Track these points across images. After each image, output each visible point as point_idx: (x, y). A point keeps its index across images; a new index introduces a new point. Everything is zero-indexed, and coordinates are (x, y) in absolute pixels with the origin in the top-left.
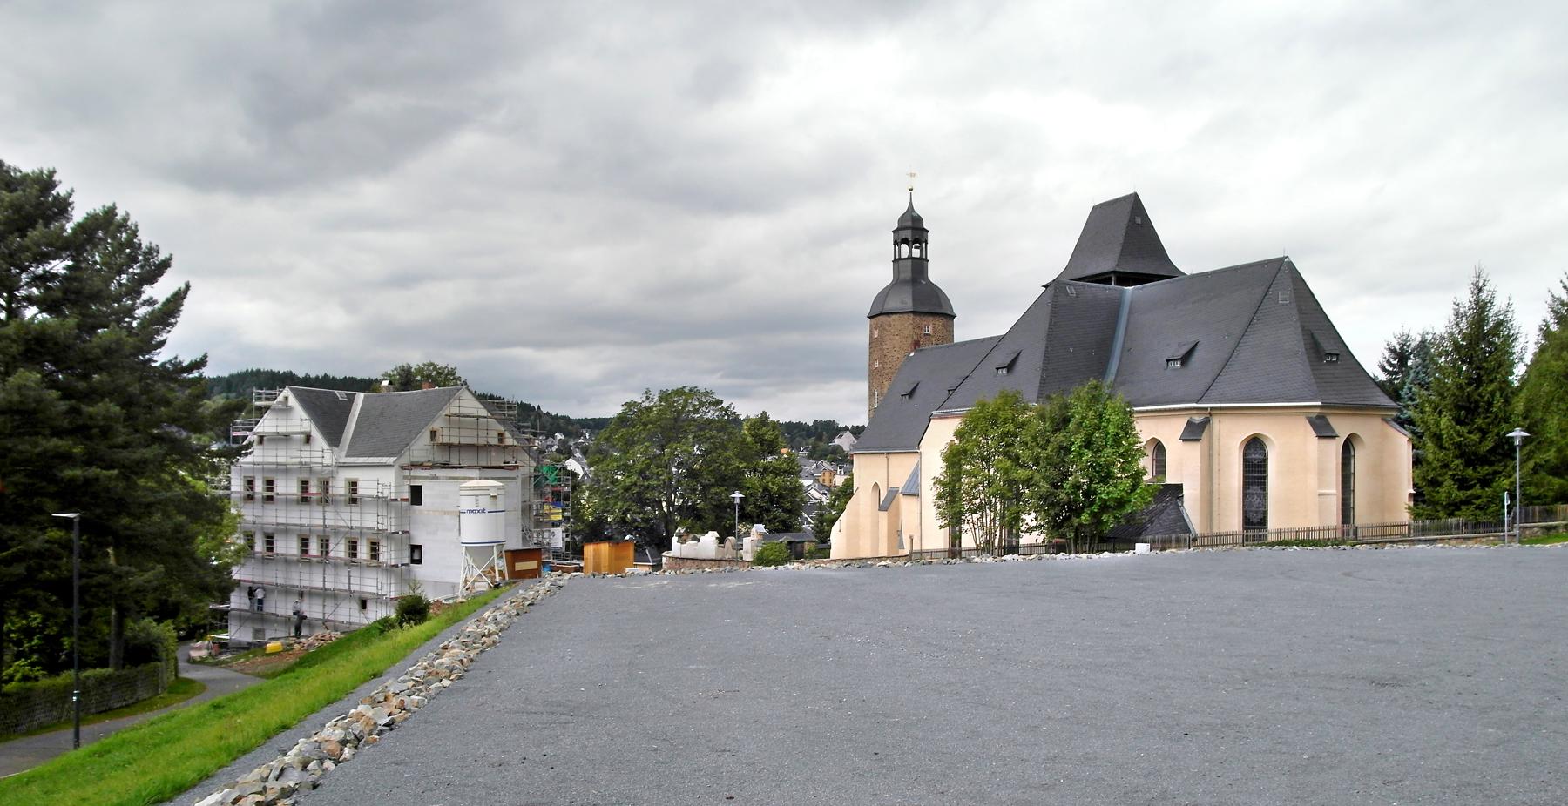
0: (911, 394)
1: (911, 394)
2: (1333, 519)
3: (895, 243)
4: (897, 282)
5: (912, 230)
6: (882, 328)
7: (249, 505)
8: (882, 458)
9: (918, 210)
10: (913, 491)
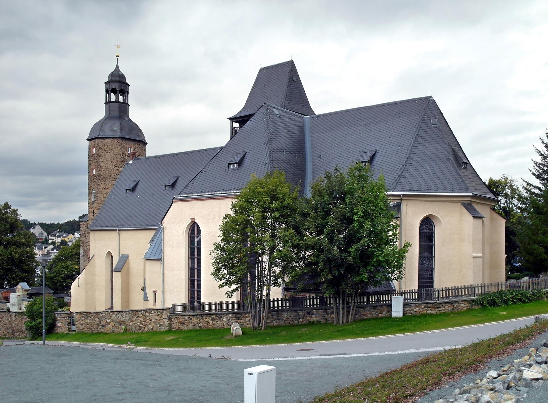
0: (134, 189)
1: (134, 189)
2: (481, 259)
3: (107, 92)
4: (108, 117)
5: (117, 85)
6: (98, 148)
7: (271, 237)
8: (114, 235)
9: (123, 70)
10: (156, 257)
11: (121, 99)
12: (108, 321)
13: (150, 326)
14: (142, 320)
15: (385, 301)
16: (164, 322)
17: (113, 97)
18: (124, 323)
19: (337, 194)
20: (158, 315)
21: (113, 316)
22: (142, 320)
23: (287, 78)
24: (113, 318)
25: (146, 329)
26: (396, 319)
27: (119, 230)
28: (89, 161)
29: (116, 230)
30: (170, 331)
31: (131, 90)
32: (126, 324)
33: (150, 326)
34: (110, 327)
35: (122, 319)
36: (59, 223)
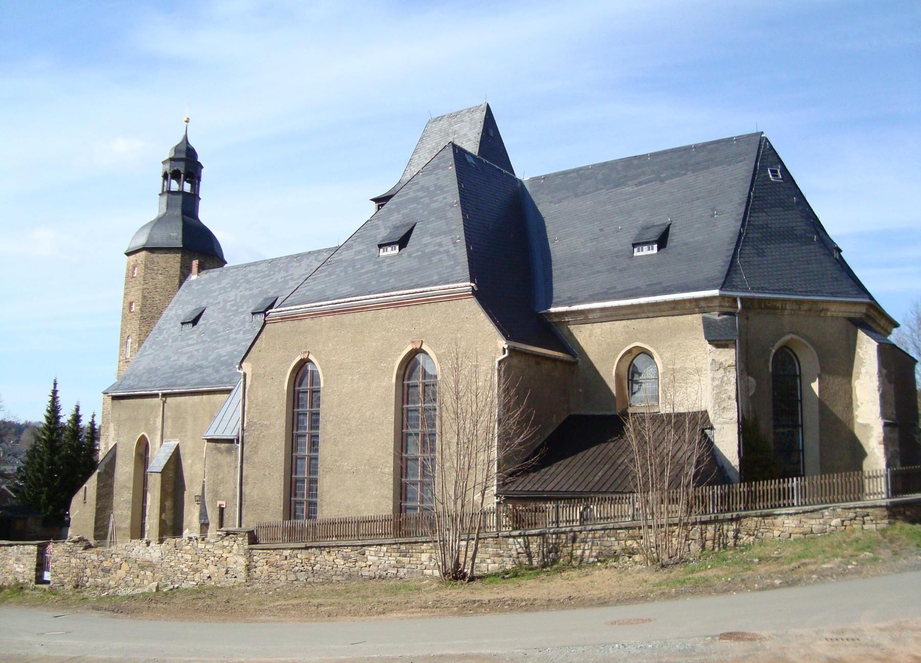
1: (195, 322)
3: (165, 176)
5: (186, 166)
9: (193, 143)
11: (187, 187)
13: (205, 571)
14: (189, 557)
17: (175, 186)
20: (224, 547)
22: (189, 557)
23: (479, 128)
27: (164, 395)
28: (126, 289)
29: (156, 395)
30: (601, 518)
31: (204, 173)
33: (205, 571)
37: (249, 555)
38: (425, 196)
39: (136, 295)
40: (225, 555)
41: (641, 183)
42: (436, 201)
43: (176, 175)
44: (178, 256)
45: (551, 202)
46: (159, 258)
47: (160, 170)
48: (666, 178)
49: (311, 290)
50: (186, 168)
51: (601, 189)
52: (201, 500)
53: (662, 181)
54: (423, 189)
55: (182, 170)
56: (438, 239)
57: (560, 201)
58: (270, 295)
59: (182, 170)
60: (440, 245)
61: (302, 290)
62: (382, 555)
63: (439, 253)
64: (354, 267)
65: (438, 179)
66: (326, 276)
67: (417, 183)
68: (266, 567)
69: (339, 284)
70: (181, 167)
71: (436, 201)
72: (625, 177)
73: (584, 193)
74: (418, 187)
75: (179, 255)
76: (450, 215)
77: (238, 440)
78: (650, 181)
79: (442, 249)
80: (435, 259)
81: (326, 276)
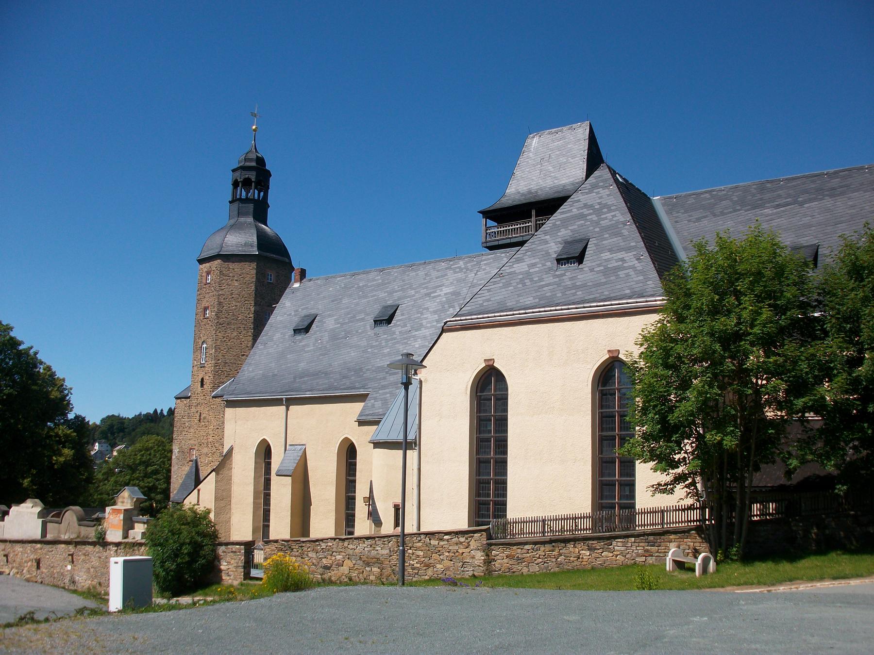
3: (236, 184)
12: (339, 557)
14: (421, 553)
15: (653, 525)
16: (473, 557)
18: (378, 561)
19: (94, 507)
21: (351, 546)
22: (421, 553)
23: (585, 145)
24: (351, 552)
25: (430, 572)
26: (249, 573)
32: (382, 563)
33: (438, 566)
34: (345, 569)
35: (374, 553)
36: (140, 414)
37: (487, 549)
38: (590, 214)
39: (210, 300)
40: (460, 551)
41: (778, 206)
42: (606, 218)
43: (247, 183)
44: (254, 265)
45: (689, 221)
46: (236, 267)
47: (229, 178)
48: (805, 202)
49: (488, 300)
50: (256, 178)
51: (739, 210)
52: (370, 500)
53: (801, 204)
54: (586, 206)
55: (253, 179)
56: (620, 255)
57: (698, 220)
58: (389, 303)
59: (253, 179)
60: (622, 260)
61: (479, 300)
62: (630, 545)
63: (625, 268)
64: (531, 280)
65: (601, 198)
66: (501, 288)
67: (579, 201)
68: (506, 561)
69: (519, 295)
70: (252, 176)
71: (606, 218)
72: (761, 199)
73: (722, 214)
74: (580, 204)
75: (254, 265)
76: (625, 232)
77: (415, 443)
78: (787, 204)
79: (625, 265)
80: (622, 274)
81: (501, 288)
